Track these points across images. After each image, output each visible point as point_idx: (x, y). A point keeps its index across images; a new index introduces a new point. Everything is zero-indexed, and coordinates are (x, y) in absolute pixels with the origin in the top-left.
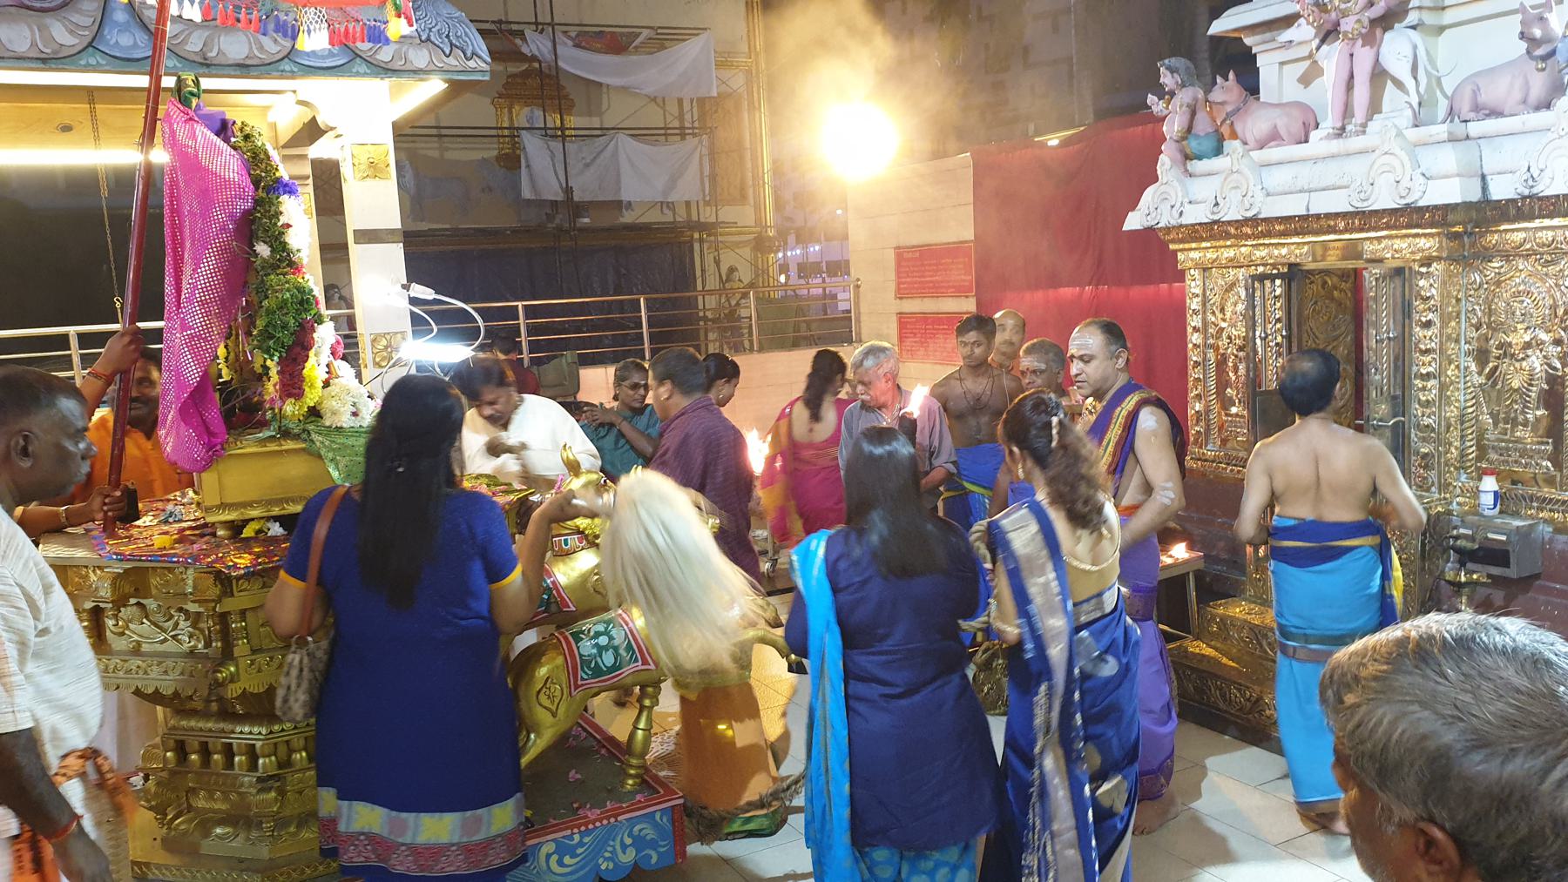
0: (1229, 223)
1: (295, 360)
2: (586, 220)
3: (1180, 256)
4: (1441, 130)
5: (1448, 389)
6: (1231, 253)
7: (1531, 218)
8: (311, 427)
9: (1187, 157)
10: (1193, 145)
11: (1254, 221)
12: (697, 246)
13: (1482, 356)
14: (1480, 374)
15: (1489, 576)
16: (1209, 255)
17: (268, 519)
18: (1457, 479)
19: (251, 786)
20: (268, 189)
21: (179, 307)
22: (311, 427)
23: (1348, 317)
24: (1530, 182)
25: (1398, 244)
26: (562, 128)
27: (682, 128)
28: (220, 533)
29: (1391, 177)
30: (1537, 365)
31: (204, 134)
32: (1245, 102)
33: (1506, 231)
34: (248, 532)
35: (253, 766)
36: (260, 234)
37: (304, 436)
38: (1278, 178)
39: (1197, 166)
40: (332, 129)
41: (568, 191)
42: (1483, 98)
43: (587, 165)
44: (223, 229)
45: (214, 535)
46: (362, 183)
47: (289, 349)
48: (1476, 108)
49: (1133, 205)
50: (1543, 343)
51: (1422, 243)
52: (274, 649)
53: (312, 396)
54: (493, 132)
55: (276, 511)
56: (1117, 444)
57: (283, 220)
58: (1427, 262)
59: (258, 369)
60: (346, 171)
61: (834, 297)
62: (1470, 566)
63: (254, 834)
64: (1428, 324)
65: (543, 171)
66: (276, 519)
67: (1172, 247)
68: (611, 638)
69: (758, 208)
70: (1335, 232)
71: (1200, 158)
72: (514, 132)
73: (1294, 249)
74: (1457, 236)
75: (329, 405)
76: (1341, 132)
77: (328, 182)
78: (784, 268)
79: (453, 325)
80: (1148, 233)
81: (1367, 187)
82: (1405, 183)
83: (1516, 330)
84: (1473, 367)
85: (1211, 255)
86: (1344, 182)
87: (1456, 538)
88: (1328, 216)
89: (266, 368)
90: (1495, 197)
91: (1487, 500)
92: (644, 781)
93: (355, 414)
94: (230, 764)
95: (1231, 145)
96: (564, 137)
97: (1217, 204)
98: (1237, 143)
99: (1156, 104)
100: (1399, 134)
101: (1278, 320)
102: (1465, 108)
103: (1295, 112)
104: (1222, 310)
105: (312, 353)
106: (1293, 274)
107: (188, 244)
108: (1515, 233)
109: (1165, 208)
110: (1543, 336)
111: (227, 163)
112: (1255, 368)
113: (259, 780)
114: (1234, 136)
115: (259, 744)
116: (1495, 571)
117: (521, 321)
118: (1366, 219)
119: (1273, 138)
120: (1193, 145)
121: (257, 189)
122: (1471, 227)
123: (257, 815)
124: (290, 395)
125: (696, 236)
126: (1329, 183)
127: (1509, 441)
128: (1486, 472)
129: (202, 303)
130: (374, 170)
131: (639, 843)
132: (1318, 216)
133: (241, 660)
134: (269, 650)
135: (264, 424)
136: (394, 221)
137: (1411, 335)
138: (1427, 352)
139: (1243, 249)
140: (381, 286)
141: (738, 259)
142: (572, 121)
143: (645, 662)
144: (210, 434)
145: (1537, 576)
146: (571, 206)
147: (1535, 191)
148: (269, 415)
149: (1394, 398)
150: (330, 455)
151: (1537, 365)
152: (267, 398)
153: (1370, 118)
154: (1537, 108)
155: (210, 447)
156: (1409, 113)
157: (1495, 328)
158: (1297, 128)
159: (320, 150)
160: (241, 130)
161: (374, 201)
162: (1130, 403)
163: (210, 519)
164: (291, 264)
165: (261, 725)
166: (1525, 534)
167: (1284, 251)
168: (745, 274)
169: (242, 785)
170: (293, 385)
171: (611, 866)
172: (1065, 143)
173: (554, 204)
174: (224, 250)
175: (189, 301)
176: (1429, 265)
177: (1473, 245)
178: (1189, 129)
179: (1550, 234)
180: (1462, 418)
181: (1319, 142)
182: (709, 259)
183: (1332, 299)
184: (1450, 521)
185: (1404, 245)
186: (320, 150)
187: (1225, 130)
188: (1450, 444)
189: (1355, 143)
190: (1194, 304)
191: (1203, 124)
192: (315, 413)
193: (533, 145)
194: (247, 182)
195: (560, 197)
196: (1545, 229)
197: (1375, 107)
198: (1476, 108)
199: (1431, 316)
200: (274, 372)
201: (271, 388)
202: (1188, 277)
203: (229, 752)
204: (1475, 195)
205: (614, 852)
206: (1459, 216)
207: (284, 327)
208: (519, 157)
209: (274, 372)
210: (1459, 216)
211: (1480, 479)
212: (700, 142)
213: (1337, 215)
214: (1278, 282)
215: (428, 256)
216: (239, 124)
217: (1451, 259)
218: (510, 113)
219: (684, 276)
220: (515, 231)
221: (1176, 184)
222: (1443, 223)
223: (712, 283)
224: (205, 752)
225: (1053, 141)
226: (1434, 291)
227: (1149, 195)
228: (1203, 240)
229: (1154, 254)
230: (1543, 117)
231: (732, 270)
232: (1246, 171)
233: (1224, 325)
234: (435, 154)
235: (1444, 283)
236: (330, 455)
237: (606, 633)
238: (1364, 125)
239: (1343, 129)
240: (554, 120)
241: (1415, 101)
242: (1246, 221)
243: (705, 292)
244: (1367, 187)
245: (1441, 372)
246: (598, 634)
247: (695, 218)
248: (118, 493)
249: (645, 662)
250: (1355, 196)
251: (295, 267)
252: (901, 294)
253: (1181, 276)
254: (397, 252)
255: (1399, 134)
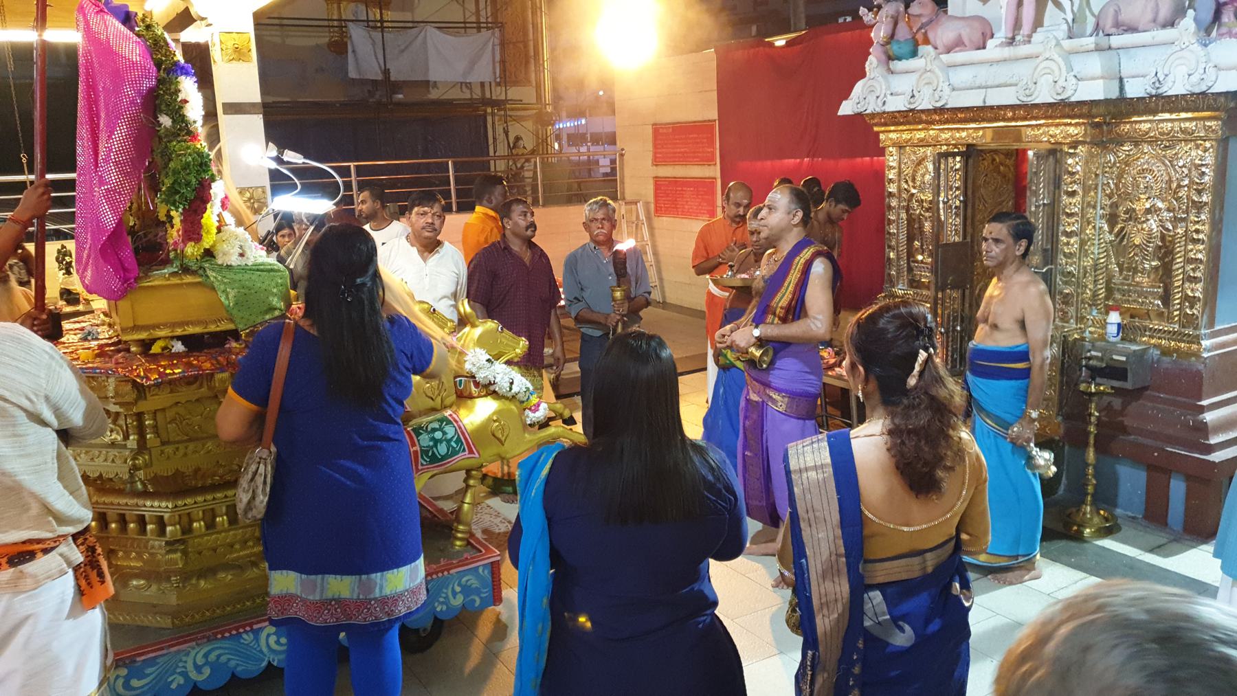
0: (923, 111)
1: (195, 211)
2: (401, 96)
3: (882, 137)
4: (1089, 42)
5: (1085, 240)
6: (921, 135)
7: (1155, 113)
8: (207, 265)
9: (890, 58)
10: (895, 48)
11: (940, 110)
12: (489, 119)
13: (1112, 219)
14: (1110, 233)
15: (1112, 388)
16: (904, 136)
17: (172, 338)
18: (1090, 314)
19: (160, 547)
20: (168, 71)
21: (96, 166)
22: (207, 265)
23: (1010, 187)
24: (1157, 85)
25: (1053, 130)
26: (382, 21)
27: (479, 22)
28: (133, 349)
29: (1050, 78)
30: (1154, 226)
31: (115, 24)
32: (937, 15)
33: (1136, 122)
34: (156, 349)
35: (161, 530)
36: (163, 107)
37: (201, 272)
38: (962, 77)
39: (897, 65)
40: (203, 19)
41: (386, 72)
42: (1123, 17)
43: (403, 51)
44: (133, 102)
45: (128, 350)
46: (228, 65)
47: (191, 202)
48: (1117, 25)
49: (846, 95)
50: (1160, 209)
51: (1071, 130)
52: (178, 442)
53: (208, 241)
54: (326, 23)
55: (179, 332)
56: (797, 285)
57: (181, 96)
58: (1074, 145)
59: (162, 217)
60: (215, 54)
61: (597, 162)
62: (1098, 380)
63: (165, 585)
64: (1072, 194)
65: (365, 57)
66: (179, 338)
67: (876, 129)
68: (444, 433)
69: (539, 87)
70: (1004, 120)
71: (899, 59)
72: (342, 25)
73: (969, 133)
74: (1098, 125)
75: (220, 249)
76: (1011, 41)
77: (199, 60)
78: (558, 138)
79: (313, 182)
80: (858, 119)
81: (1031, 85)
82: (1061, 83)
83: (1139, 199)
84: (1106, 227)
85: (905, 136)
86: (1013, 81)
87: (1090, 358)
88: (1000, 107)
89: (170, 218)
90: (1129, 96)
91: (1112, 329)
92: (469, 543)
93: (242, 255)
94: (143, 530)
95: (923, 49)
96: (382, 28)
97: (913, 96)
98: (929, 48)
99: (866, 15)
100: (1058, 44)
101: (957, 188)
102: (1108, 23)
103: (976, 24)
104: (914, 180)
105: (209, 206)
106: (970, 153)
107: (103, 115)
108: (1143, 124)
109: (871, 98)
110: (1160, 205)
111: (131, 49)
112: (939, 225)
113: (167, 543)
114: (927, 41)
115: (166, 516)
116: (1116, 384)
117: (353, 178)
118: (1028, 110)
119: (957, 44)
120: (895, 48)
121: (159, 70)
122: (1109, 119)
123: (166, 571)
124: (190, 239)
125: (489, 110)
126: (1002, 81)
127: (1129, 285)
128: (1115, 308)
129: (116, 163)
130: (239, 54)
131: (467, 590)
132: (992, 107)
133: (153, 451)
134: (175, 443)
135: (166, 262)
136: (255, 96)
137: (1060, 202)
138: (1070, 215)
139: (931, 132)
140: (245, 154)
141: (525, 131)
142: (389, 15)
143: (471, 452)
144: (125, 270)
145: (1145, 388)
146: (388, 84)
147: (1160, 91)
148: (172, 255)
149: (1045, 251)
150: (222, 287)
151: (1154, 226)
152: (170, 241)
153: (1034, 30)
154: (1164, 26)
155: (125, 280)
156: (1065, 27)
157: (1128, 197)
158: (977, 36)
159: (190, 35)
160: (143, 20)
161: (239, 79)
162: (807, 253)
163: (125, 338)
164: (189, 133)
165: (168, 500)
166: (1140, 356)
167: (964, 134)
168: (528, 143)
169: (153, 547)
170: (193, 231)
171: (445, 608)
172: (790, 43)
173: (374, 82)
174: (133, 119)
175: (106, 161)
176: (1075, 148)
177: (1110, 132)
178: (892, 36)
179: (1170, 125)
180: (1095, 267)
181: (994, 49)
182: (499, 130)
183: (999, 172)
184: (1083, 346)
185: (1058, 132)
186: (190, 35)
187: (919, 37)
188: (1086, 286)
189: (1023, 50)
190: (891, 175)
191: (903, 32)
192: (209, 254)
193: (357, 34)
194: (150, 65)
195: (380, 77)
196: (1167, 121)
197: (1038, 23)
198: (1117, 25)
199: (1075, 187)
200: (177, 221)
201: (174, 234)
202: (887, 152)
203: (142, 521)
204: (1114, 94)
205: (447, 597)
206: (1102, 110)
207: (188, 184)
208: (346, 44)
209: (177, 221)
210: (1102, 110)
211: (1107, 313)
212: (493, 34)
213: (1006, 107)
214: (958, 159)
215: (282, 124)
216: (140, 15)
217: (1093, 143)
218: (339, 8)
219: (479, 144)
220: (343, 104)
221: (880, 79)
222: (1090, 116)
223: (502, 150)
224: (123, 521)
225: (780, 42)
226: (1078, 168)
227: (859, 87)
228: (901, 124)
229: (862, 133)
230: (1168, 33)
231: (518, 139)
232: (937, 70)
233: (914, 191)
234: (278, 40)
235: (1087, 162)
236: (222, 287)
237: (441, 429)
238: (1030, 36)
239: (1013, 38)
240: (375, 14)
241: (1070, 17)
242: (937, 111)
243: (496, 158)
244: (1031, 85)
245: (1082, 230)
246: (434, 430)
247: (488, 95)
248: (44, 317)
249: (471, 452)
250: (1021, 92)
251: (193, 136)
252: (657, 161)
253: (882, 152)
254: (257, 121)
255: (1058, 44)
